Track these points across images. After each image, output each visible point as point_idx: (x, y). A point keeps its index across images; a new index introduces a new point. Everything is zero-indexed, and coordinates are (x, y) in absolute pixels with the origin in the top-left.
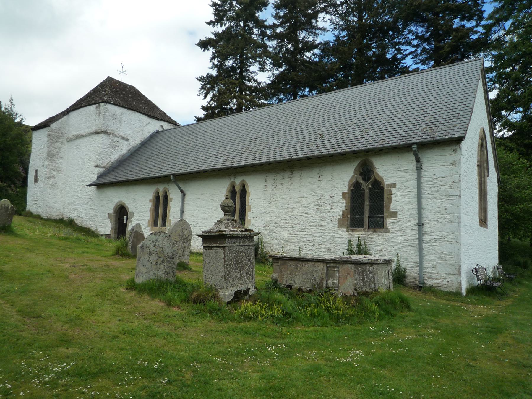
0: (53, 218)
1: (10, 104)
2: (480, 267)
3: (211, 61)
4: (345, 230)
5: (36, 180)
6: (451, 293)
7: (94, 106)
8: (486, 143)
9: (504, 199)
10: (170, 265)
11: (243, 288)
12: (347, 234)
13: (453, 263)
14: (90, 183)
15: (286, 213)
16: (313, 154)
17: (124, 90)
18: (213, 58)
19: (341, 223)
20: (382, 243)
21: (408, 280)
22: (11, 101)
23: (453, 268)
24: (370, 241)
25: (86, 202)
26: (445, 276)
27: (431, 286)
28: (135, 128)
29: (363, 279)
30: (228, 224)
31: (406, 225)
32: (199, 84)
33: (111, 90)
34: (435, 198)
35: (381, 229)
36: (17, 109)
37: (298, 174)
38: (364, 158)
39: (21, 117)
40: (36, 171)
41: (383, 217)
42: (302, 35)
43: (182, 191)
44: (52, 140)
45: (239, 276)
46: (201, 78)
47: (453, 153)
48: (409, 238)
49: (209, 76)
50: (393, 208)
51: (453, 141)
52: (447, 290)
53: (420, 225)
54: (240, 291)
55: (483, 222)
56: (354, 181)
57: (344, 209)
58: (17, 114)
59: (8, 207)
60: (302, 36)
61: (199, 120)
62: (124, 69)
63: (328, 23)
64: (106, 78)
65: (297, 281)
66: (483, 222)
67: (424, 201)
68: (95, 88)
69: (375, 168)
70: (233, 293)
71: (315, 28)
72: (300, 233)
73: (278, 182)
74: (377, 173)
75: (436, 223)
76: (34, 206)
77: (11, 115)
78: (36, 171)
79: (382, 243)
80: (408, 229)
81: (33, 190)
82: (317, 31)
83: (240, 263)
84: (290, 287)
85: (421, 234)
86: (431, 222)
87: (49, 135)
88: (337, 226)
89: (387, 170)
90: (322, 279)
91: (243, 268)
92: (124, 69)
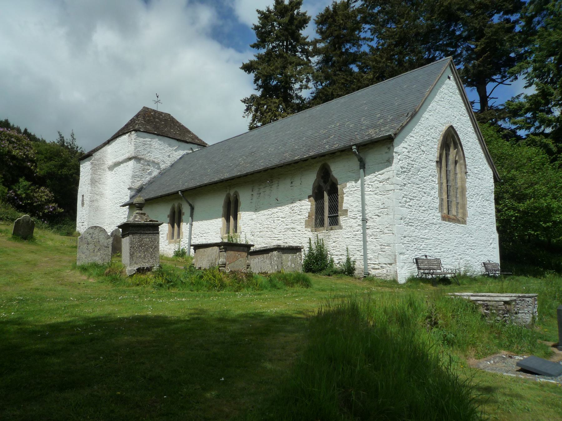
3: (255, 82)
4: (310, 230)
5: (83, 204)
7: (127, 135)
8: (459, 139)
10: (106, 252)
11: (146, 265)
13: (390, 253)
15: (267, 219)
17: (158, 118)
18: (256, 80)
20: (337, 239)
21: (356, 272)
22: (72, 135)
23: (390, 258)
24: (328, 238)
26: (384, 265)
28: (164, 153)
29: (271, 263)
31: (354, 221)
32: (244, 106)
33: (144, 118)
34: (376, 194)
35: (336, 227)
37: (288, 181)
38: (323, 163)
40: (83, 196)
43: (190, 205)
45: (142, 256)
46: (245, 100)
48: (357, 233)
49: (253, 98)
50: (345, 206)
51: (384, 140)
54: (144, 268)
58: (77, 147)
59: (29, 222)
64: (140, 108)
67: (367, 197)
70: (135, 269)
71: (359, 38)
72: (277, 236)
73: (262, 191)
74: (332, 175)
75: (377, 217)
78: (83, 196)
79: (337, 239)
80: (356, 225)
82: (360, 43)
83: (145, 246)
85: (364, 228)
86: (373, 217)
87: (92, 163)
88: (304, 227)
89: (337, 170)
91: (147, 250)
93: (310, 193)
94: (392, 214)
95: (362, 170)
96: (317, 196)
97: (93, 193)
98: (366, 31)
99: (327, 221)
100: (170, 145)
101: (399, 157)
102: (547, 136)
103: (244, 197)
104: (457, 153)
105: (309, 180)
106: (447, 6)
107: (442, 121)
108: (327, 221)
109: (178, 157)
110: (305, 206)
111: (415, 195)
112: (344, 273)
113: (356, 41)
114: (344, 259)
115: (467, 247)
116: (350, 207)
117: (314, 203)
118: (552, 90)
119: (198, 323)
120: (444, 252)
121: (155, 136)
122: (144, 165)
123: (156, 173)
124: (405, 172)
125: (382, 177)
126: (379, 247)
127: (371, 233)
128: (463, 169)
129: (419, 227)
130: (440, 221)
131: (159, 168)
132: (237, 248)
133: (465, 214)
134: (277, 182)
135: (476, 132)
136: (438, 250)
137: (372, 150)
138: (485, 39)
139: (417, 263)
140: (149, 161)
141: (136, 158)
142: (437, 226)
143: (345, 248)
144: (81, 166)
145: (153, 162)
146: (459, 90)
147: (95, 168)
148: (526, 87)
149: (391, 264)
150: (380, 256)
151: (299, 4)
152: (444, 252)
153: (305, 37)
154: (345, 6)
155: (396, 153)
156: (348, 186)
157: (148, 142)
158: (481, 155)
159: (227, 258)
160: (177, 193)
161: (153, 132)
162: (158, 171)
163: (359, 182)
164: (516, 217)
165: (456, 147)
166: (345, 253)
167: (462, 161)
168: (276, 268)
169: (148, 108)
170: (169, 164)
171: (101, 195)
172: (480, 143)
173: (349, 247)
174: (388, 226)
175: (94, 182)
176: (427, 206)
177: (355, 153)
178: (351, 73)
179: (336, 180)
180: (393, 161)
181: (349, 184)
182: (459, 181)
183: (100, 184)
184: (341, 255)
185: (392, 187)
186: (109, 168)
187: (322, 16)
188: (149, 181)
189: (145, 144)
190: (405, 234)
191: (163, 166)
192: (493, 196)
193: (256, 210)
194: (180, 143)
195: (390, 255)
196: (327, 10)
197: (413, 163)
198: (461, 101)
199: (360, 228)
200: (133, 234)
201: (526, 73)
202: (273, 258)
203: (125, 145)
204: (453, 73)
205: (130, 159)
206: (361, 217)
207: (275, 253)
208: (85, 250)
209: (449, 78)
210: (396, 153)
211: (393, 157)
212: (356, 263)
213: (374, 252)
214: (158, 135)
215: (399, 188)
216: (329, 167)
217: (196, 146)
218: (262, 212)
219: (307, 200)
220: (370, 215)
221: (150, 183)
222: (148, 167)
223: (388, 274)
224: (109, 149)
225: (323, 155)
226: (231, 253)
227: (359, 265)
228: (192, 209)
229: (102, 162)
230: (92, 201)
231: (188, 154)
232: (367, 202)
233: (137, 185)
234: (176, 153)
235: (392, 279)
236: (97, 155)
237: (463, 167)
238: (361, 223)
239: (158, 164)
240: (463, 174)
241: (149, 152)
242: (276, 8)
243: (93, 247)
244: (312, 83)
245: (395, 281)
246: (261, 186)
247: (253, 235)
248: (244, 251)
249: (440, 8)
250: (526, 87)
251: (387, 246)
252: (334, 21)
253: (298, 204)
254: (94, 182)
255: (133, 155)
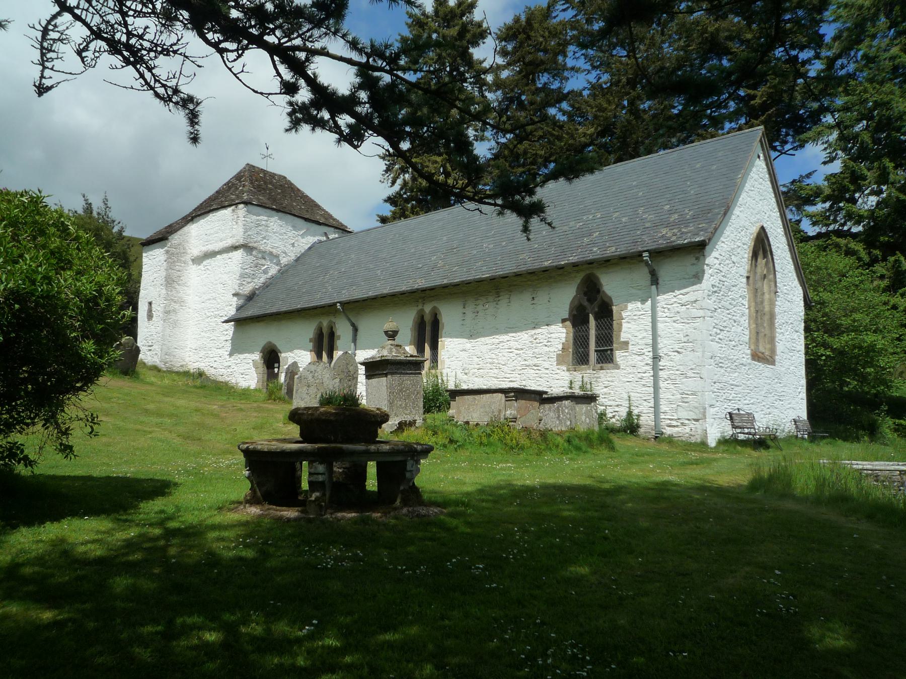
0: (175, 369)
1: (103, 206)
2: (742, 412)
4: (565, 369)
5: (150, 316)
6: (695, 444)
7: (230, 209)
8: (770, 245)
9: (817, 324)
11: (408, 418)
12: (567, 374)
13: (696, 405)
14: (226, 318)
15: (491, 350)
16: (523, 268)
17: (271, 183)
19: (560, 360)
21: (642, 431)
22: (105, 201)
25: (221, 346)
26: (687, 422)
27: (671, 437)
28: (287, 239)
29: (559, 416)
30: (391, 349)
31: (640, 358)
33: (252, 183)
36: (113, 214)
37: (527, 296)
38: (588, 272)
39: (120, 225)
40: (150, 303)
41: (612, 350)
42: (544, 78)
43: (353, 325)
44: (173, 260)
47: (695, 262)
50: (624, 337)
52: (693, 440)
53: (656, 358)
55: (763, 355)
56: (576, 303)
57: (564, 340)
60: (542, 82)
61: (384, 220)
62: (270, 152)
63: (582, 59)
65: (475, 415)
66: (763, 355)
67: (660, 326)
68: (229, 182)
69: (601, 285)
70: (397, 423)
71: (564, 67)
73: (480, 308)
76: (148, 353)
77: (106, 223)
78: (150, 303)
80: (643, 364)
81: (146, 330)
82: (566, 74)
84: (467, 423)
85: (655, 368)
86: (670, 353)
87: (167, 252)
89: (611, 284)
90: (500, 411)
92: (270, 152)
93: (566, 315)
94: (701, 350)
95: (654, 287)
96: (578, 319)
97: (169, 299)
98: (574, 58)
99: (593, 356)
100: (295, 227)
101: (710, 271)
102: (854, 236)
103: (449, 314)
104: (767, 264)
105: (565, 296)
106: (712, 34)
107: (753, 220)
108: (593, 356)
109: (307, 247)
110: (559, 334)
111: (725, 324)
112: (626, 432)
113: (558, 71)
114: (623, 412)
115: (776, 397)
116: (633, 338)
117: (571, 329)
118: (865, 172)
119: (495, 497)
120: (752, 404)
121: (274, 212)
122: (257, 258)
123: (273, 270)
124: (715, 292)
125: (691, 297)
126: (679, 396)
127: (666, 377)
128: (773, 288)
129: (729, 369)
130: (750, 361)
131: (278, 264)
132: (528, 395)
133: (773, 351)
134: (507, 296)
135: (786, 234)
136: (747, 402)
137: (675, 257)
138: (769, 88)
139: (731, 419)
140: (265, 252)
141: (247, 247)
142: (747, 368)
143: (626, 397)
144: (144, 255)
145: (271, 253)
146: (770, 174)
147: (173, 260)
148: (825, 163)
149: (697, 420)
150: (680, 409)
151: (472, 6)
152: (752, 404)
153: (482, 59)
154: (544, 16)
155: (708, 265)
156: (629, 308)
157: (264, 223)
158: (791, 267)
159: (519, 410)
160: (335, 304)
161: (270, 206)
162: (278, 268)
163: (649, 303)
164: (828, 357)
165: (765, 256)
166: (626, 404)
167: (772, 276)
168: (569, 423)
169: (254, 167)
170: (292, 257)
171: (181, 302)
172: (790, 251)
173: (632, 394)
174: (693, 367)
175: (170, 282)
176: (736, 339)
177: (646, 262)
178: (555, 123)
179: (610, 299)
180: (703, 276)
181: (630, 306)
182: (766, 303)
183: (179, 285)
184: (617, 406)
185: (701, 313)
186: (193, 260)
187: (509, 28)
188: (264, 284)
189: (259, 225)
190: (716, 378)
191: (284, 261)
192: (803, 325)
193: (471, 336)
194: (309, 225)
195: (696, 408)
196: (517, 20)
197: (724, 279)
198: (771, 190)
199: (649, 368)
200: (392, 374)
201: (826, 142)
202: (563, 411)
203: (226, 225)
204: (763, 150)
205: (235, 248)
206: (651, 354)
207: (567, 403)
208: (305, 396)
209: (759, 157)
210: (708, 265)
211: (703, 272)
212: (641, 418)
213: (671, 403)
214: (278, 211)
215: (710, 314)
216: (598, 279)
217: (332, 229)
218: (483, 339)
219: (561, 325)
220: (665, 350)
221: (266, 286)
222: (263, 261)
223: (693, 433)
224: (194, 230)
225: (591, 263)
226: (522, 402)
227: (646, 421)
228: (356, 330)
229: (182, 251)
230: (167, 312)
231: (320, 242)
232: (660, 332)
233: (247, 289)
234: (304, 240)
235: (699, 440)
236: (175, 239)
237: (773, 284)
238: (650, 361)
239: (277, 256)
240: (773, 294)
241: (264, 238)
242: (436, 11)
243: (316, 390)
244: (490, 133)
245: (704, 444)
246: (479, 302)
247: (466, 374)
248: (535, 401)
249: (702, 34)
250: (825, 163)
251: (692, 394)
252: (529, 38)
253: (544, 330)
254: (170, 282)
255: (241, 242)
